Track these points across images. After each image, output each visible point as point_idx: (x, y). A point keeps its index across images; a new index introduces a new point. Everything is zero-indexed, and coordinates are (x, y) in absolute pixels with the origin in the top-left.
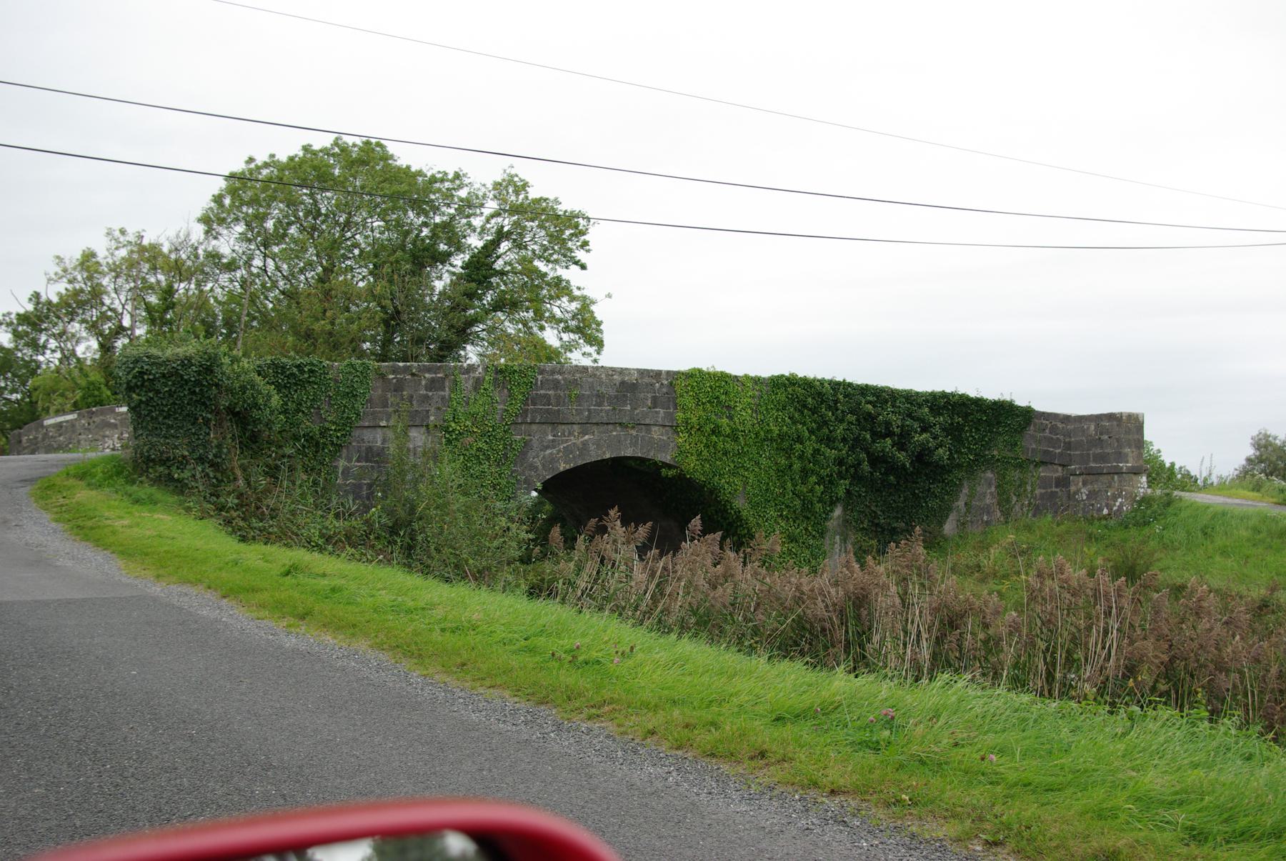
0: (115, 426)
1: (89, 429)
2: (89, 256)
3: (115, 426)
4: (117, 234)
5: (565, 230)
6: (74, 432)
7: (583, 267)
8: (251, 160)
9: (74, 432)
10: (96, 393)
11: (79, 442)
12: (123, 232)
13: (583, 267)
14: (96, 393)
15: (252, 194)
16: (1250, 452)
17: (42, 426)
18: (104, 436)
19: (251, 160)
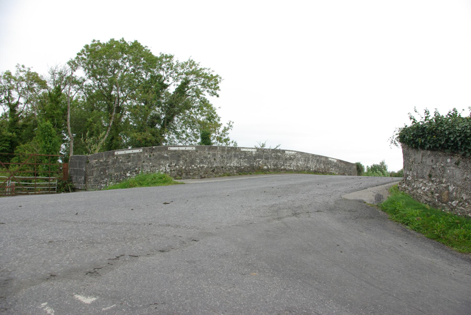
0: (167, 158)
1: (150, 160)
2: (9, 74)
3: (167, 158)
4: (21, 67)
5: (212, 82)
6: (139, 160)
7: (218, 96)
8: (94, 41)
9: (139, 160)
10: (49, 130)
11: (143, 166)
12: (23, 66)
13: (218, 96)
14: (49, 130)
15: (99, 56)
16: (379, 164)
17: (113, 155)
18: (160, 164)
19: (94, 41)
